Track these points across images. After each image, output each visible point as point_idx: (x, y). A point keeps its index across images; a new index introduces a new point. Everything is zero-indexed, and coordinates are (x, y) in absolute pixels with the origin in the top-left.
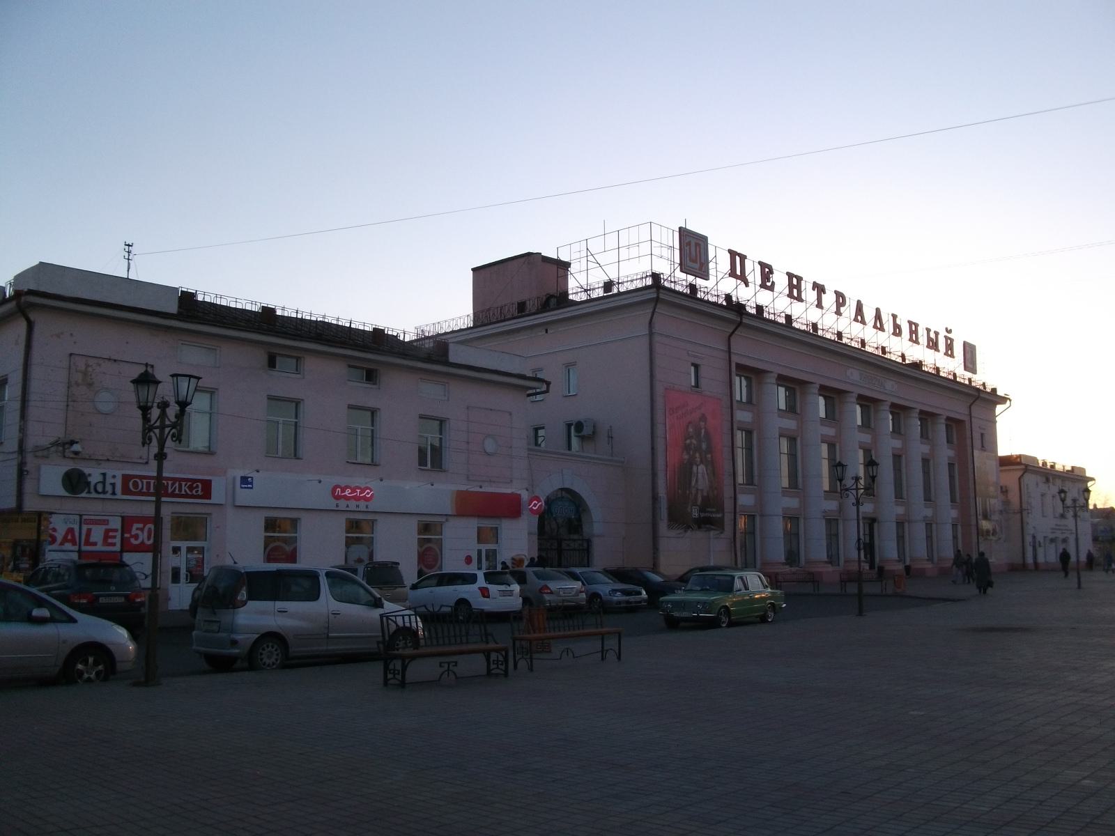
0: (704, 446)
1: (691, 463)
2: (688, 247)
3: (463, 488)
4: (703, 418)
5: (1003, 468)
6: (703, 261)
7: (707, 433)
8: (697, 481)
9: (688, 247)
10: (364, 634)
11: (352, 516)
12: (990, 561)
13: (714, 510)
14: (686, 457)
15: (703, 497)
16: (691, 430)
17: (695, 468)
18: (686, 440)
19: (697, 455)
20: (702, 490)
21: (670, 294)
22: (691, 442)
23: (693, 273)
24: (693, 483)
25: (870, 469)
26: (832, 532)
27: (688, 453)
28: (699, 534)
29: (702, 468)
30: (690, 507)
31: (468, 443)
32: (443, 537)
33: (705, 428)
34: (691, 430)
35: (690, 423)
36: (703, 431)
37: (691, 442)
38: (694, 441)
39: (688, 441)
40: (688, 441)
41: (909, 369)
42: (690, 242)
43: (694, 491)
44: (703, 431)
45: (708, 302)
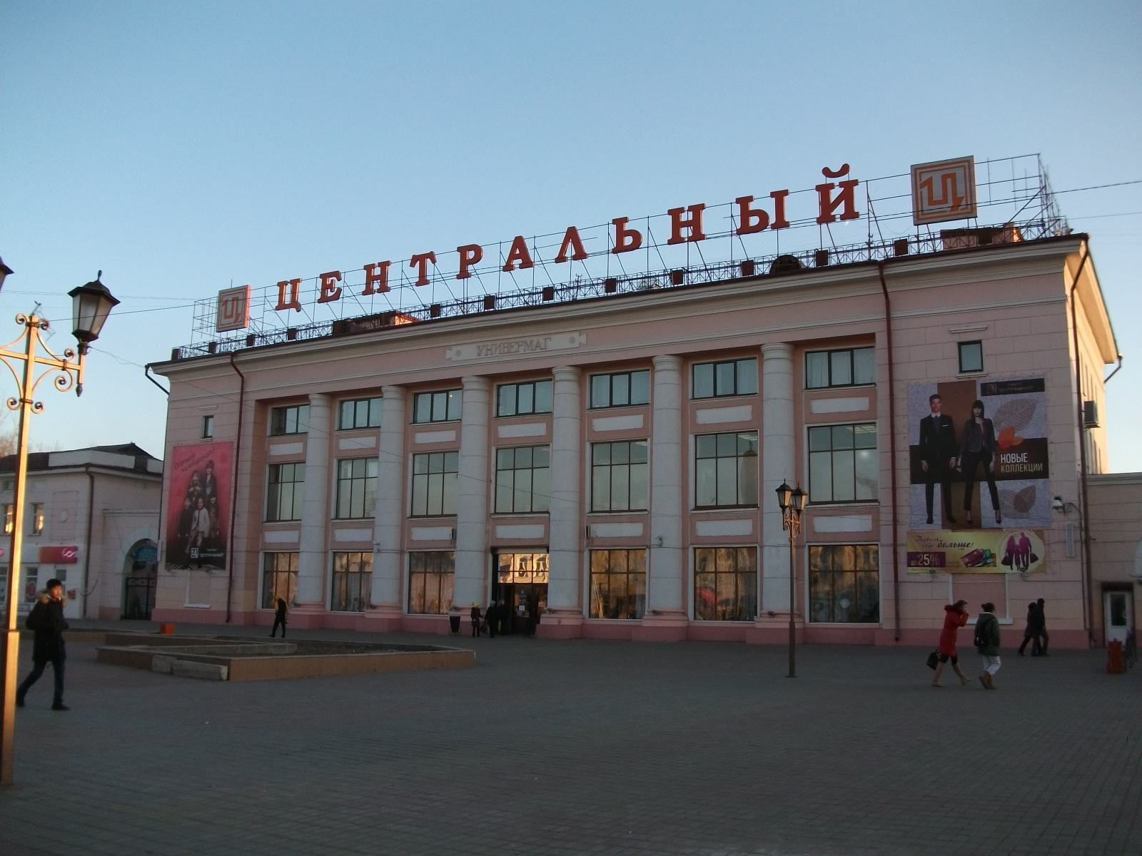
0: (208, 491)
1: (195, 507)
2: (224, 307)
3: (43, 546)
4: (211, 464)
5: (33, 473)
6: (239, 311)
7: (213, 478)
8: (198, 525)
9: (224, 307)
10: (261, 658)
11: (31, 566)
12: (1001, 621)
13: (214, 550)
14: (188, 503)
15: (204, 539)
16: (195, 478)
17: (196, 513)
18: (189, 488)
19: (200, 500)
20: (203, 532)
21: (282, 348)
22: (195, 490)
23: (962, 216)
24: (194, 526)
25: (505, 478)
26: (831, 574)
27: (191, 501)
28: (200, 574)
29: (204, 511)
30: (188, 548)
31: (52, 516)
32: (993, 614)
33: (212, 474)
34: (195, 478)
35: (195, 472)
36: (209, 477)
37: (195, 490)
38: (198, 488)
39: (192, 489)
40: (192, 489)
41: (336, 340)
42: (930, 180)
43: (193, 534)
44: (209, 477)
45: (719, 283)
